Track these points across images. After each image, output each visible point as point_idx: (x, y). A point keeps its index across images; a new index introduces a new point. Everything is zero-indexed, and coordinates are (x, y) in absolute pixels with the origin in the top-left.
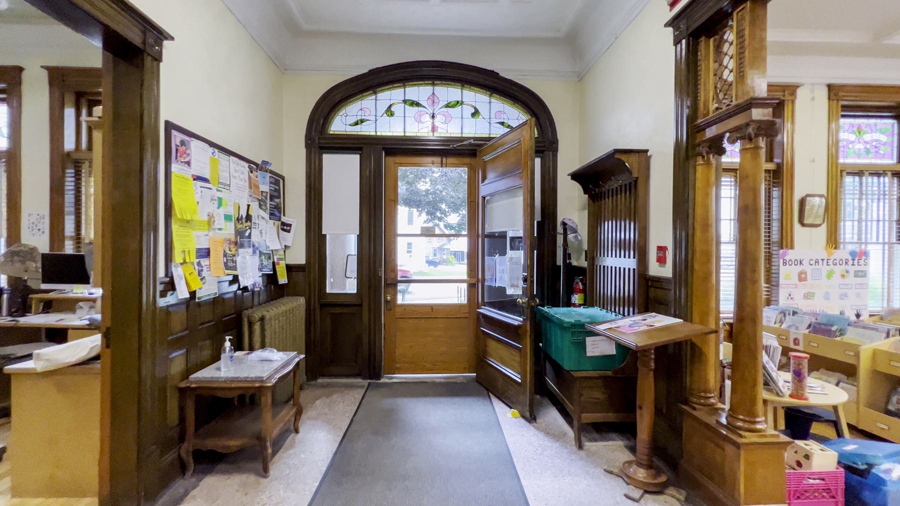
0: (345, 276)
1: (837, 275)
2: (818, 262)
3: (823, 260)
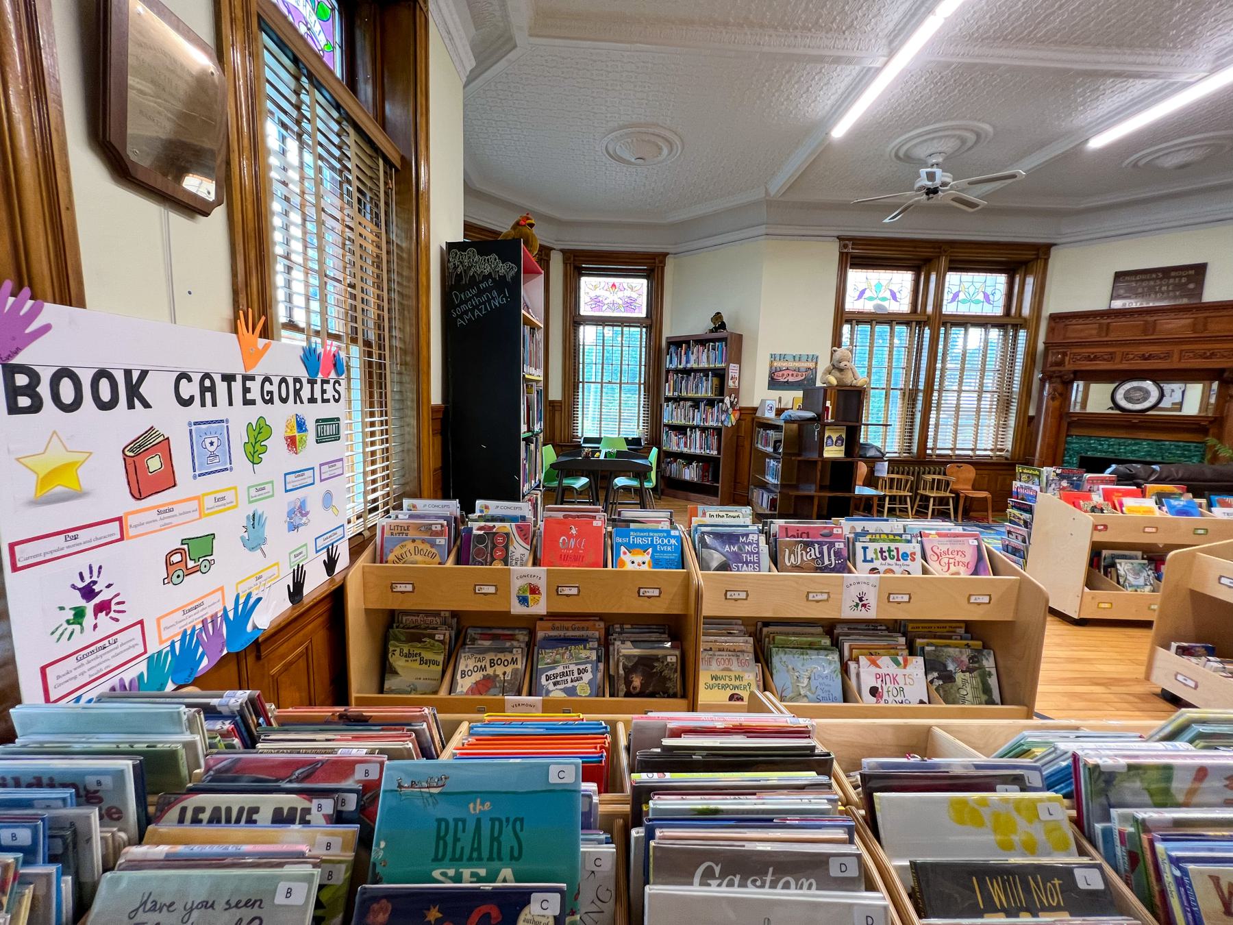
0: (239, 583)
1: (276, 444)
2: (212, 389)
3: (229, 378)
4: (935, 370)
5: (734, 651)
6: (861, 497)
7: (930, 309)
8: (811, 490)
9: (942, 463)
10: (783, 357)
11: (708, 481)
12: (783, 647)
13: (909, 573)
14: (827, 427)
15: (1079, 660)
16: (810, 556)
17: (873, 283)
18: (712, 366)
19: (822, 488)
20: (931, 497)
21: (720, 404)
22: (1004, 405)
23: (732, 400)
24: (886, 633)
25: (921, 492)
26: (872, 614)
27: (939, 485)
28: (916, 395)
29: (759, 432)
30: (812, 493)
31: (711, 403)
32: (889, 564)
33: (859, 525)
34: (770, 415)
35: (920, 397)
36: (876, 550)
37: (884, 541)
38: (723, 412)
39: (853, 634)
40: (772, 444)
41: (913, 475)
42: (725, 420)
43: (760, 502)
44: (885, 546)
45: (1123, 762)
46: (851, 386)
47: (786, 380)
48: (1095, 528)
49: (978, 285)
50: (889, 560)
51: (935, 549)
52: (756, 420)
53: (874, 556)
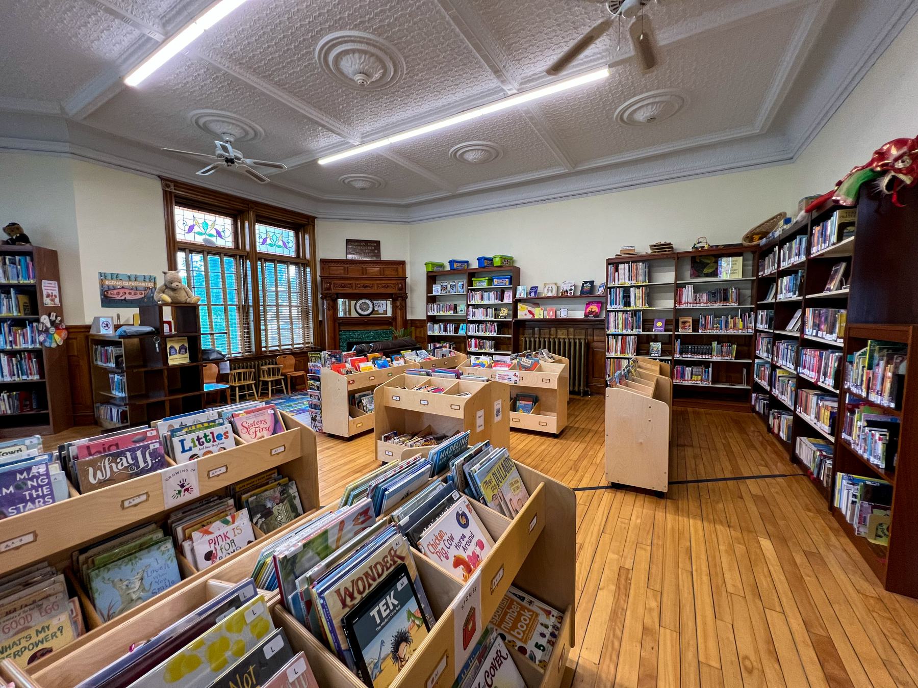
4: (258, 291)
5: (34, 602)
6: (208, 393)
7: (248, 247)
8: (161, 397)
9: (272, 357)
10: (116, 277)
11: (32, 409)
12: (95, 566)
13: (225, 449)
14: (168, 339)
15: (350, 461)
16: (122, 465)
17: (201, 221)
18: (14, 282)
19: (172, 392)
20: (236, 387)
21: (35, 324)
22: (305, 314)
23: (53, 318)
24: (218, 501)
25: (262, 379)
26: (196, 494)
27: (274, 372)
28: (248, 309)
29: (97, 349)
30: (163, 398)
31: (19, 323)
32: (207, 447)
33: (176, 422)
34: (108, 332)
35: (251, 311)
36: (193, 439)
37: (200, 429)
38: (40, 332)
39: (186, 516)
40: (113, 360)
41: (254, 368)
42: (45, 341)
43: (109, 417)
44: (201, 434)
45: (300, 544)
46: (186, 303)
47: (123, 298)
48: (349, 383)
49: (278, 235)
50: (206, 444)
51: (244, 424)
52: (90, 338)
53: (192, 445)
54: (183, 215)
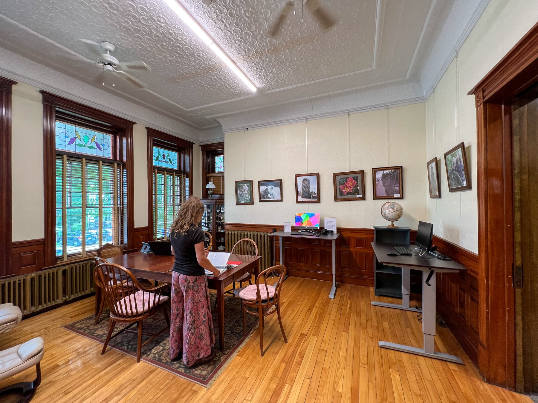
17: (162, 154)
54: (157, 151)
